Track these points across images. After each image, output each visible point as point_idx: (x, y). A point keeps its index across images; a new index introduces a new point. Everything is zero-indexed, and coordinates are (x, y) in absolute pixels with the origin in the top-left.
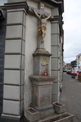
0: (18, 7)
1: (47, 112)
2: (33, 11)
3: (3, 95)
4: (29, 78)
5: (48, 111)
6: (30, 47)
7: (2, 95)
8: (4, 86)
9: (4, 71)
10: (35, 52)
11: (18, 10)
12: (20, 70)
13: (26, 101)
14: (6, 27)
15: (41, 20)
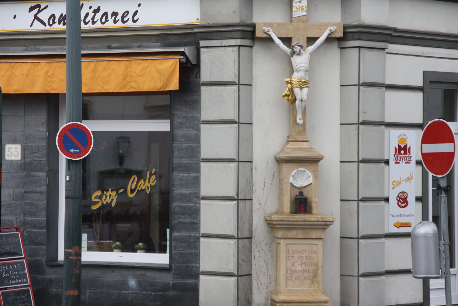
2: (269, 35)
3: (199, 264)
6: (268, 138)
7: (198, 265)
8: (202, 239)
9: (200, 203)
10: (282, 150)
11: (225, 42)
12: (236, 200)
14: (199, 92)
15: (292, 58)
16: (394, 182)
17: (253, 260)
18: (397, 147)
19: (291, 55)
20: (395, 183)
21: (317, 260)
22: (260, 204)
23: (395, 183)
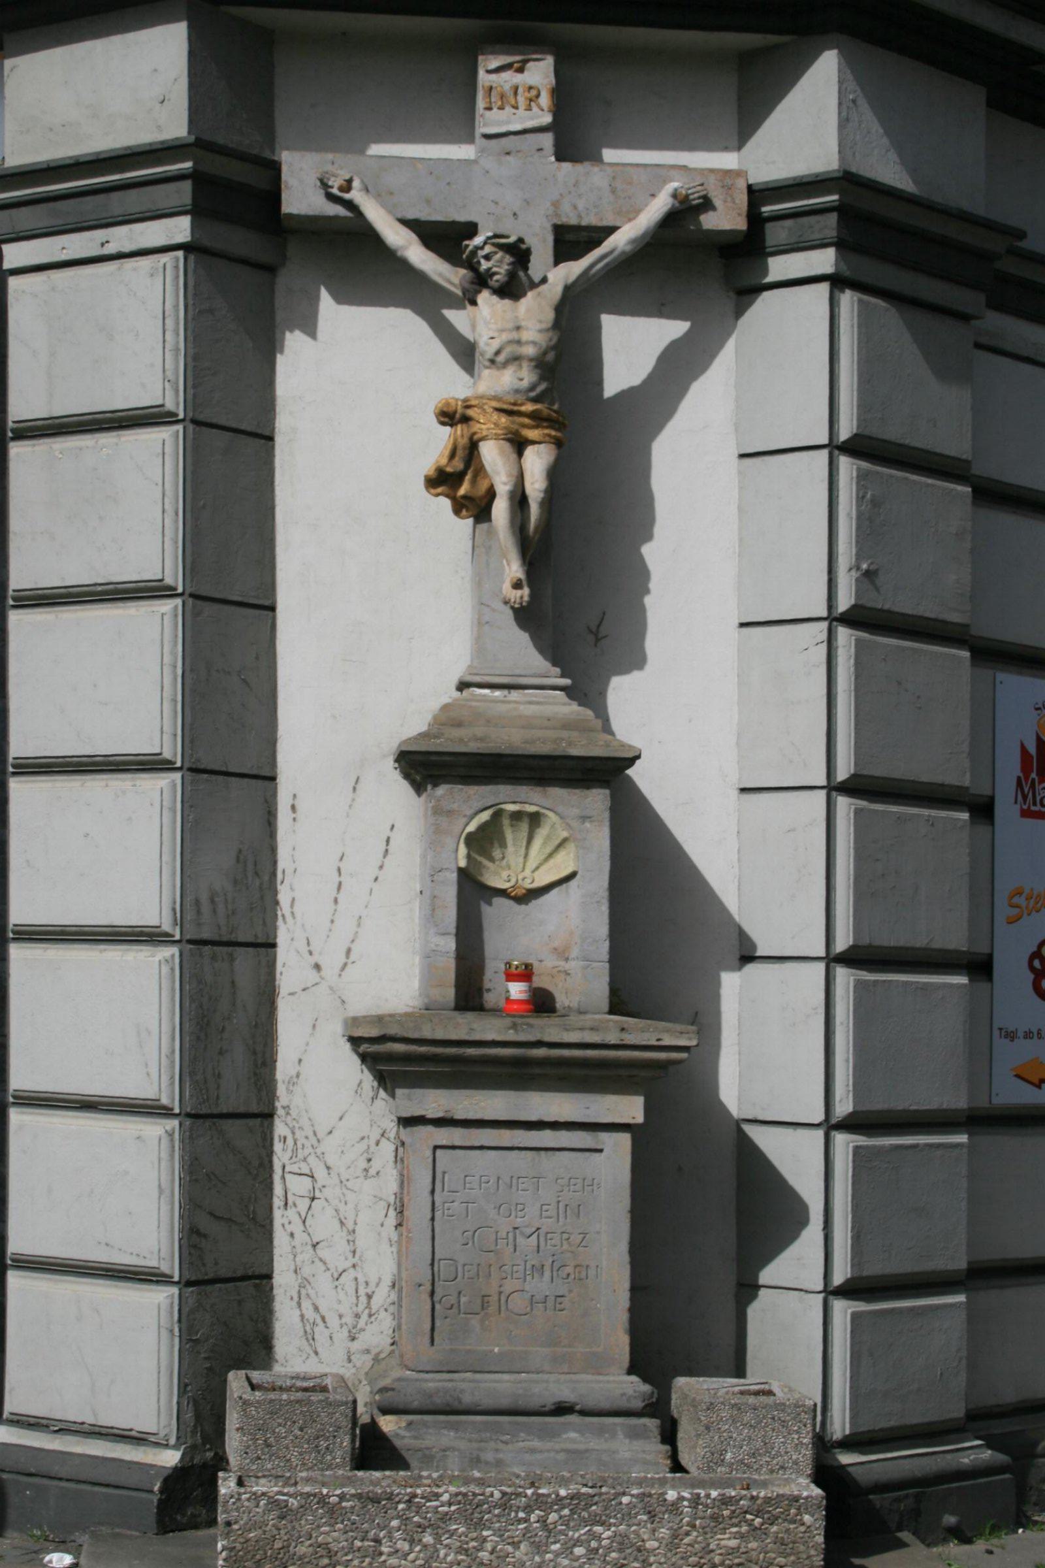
0: (119, 203)
1: (533, 1451)
2: (350, 205)
4: (355, 1041)
5: (552, 1434)
11: (121, 238)
13: (310, 1314)
16: (1019, 892)
17: (277, 1214)
18: (1032, 750)
19: (464, 291)
20: (1021, 901)
21: (1036, 1523)
22: (317, 967)
23: (1021, 901)
